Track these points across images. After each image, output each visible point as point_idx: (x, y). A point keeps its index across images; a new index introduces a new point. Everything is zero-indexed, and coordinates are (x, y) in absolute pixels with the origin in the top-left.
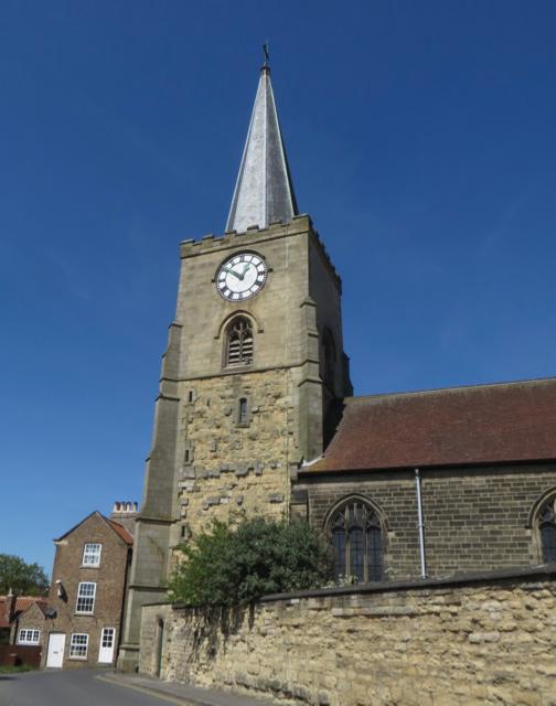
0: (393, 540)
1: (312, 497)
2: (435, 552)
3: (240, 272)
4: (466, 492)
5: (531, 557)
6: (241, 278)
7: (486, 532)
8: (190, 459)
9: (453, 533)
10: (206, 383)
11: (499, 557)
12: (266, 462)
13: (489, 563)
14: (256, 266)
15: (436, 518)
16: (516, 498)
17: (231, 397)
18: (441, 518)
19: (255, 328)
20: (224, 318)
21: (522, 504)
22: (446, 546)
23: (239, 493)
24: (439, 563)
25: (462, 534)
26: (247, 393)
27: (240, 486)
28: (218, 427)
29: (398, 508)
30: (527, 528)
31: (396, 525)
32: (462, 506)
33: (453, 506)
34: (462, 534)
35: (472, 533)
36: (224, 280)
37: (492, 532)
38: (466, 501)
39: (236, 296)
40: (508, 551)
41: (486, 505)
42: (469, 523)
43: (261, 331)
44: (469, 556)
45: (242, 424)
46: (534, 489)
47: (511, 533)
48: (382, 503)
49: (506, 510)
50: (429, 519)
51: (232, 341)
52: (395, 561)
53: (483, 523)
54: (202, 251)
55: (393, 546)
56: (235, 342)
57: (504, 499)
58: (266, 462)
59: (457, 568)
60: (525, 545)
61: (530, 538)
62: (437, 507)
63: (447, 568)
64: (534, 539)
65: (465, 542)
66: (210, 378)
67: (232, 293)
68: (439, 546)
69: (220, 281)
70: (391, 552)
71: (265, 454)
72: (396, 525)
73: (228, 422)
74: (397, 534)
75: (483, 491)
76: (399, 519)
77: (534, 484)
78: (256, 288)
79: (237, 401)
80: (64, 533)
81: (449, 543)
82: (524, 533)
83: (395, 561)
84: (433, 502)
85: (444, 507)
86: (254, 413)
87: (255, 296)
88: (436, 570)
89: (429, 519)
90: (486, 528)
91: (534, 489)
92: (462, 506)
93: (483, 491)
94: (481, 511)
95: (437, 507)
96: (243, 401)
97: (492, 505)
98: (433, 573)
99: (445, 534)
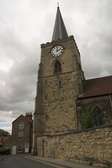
0: (105, 114)
20: (53, 61)
23: (61, 105)
26: (61, 79)
43: (63, 64)
45: (60, 87)
48: (101, 104)
52: (107, 119)
56: (57, 67)
66: (51, 76)
67: (55, 55)
69: (52, 53)
74: (106, 112)
83: (107, 119)
96: (60, 81)
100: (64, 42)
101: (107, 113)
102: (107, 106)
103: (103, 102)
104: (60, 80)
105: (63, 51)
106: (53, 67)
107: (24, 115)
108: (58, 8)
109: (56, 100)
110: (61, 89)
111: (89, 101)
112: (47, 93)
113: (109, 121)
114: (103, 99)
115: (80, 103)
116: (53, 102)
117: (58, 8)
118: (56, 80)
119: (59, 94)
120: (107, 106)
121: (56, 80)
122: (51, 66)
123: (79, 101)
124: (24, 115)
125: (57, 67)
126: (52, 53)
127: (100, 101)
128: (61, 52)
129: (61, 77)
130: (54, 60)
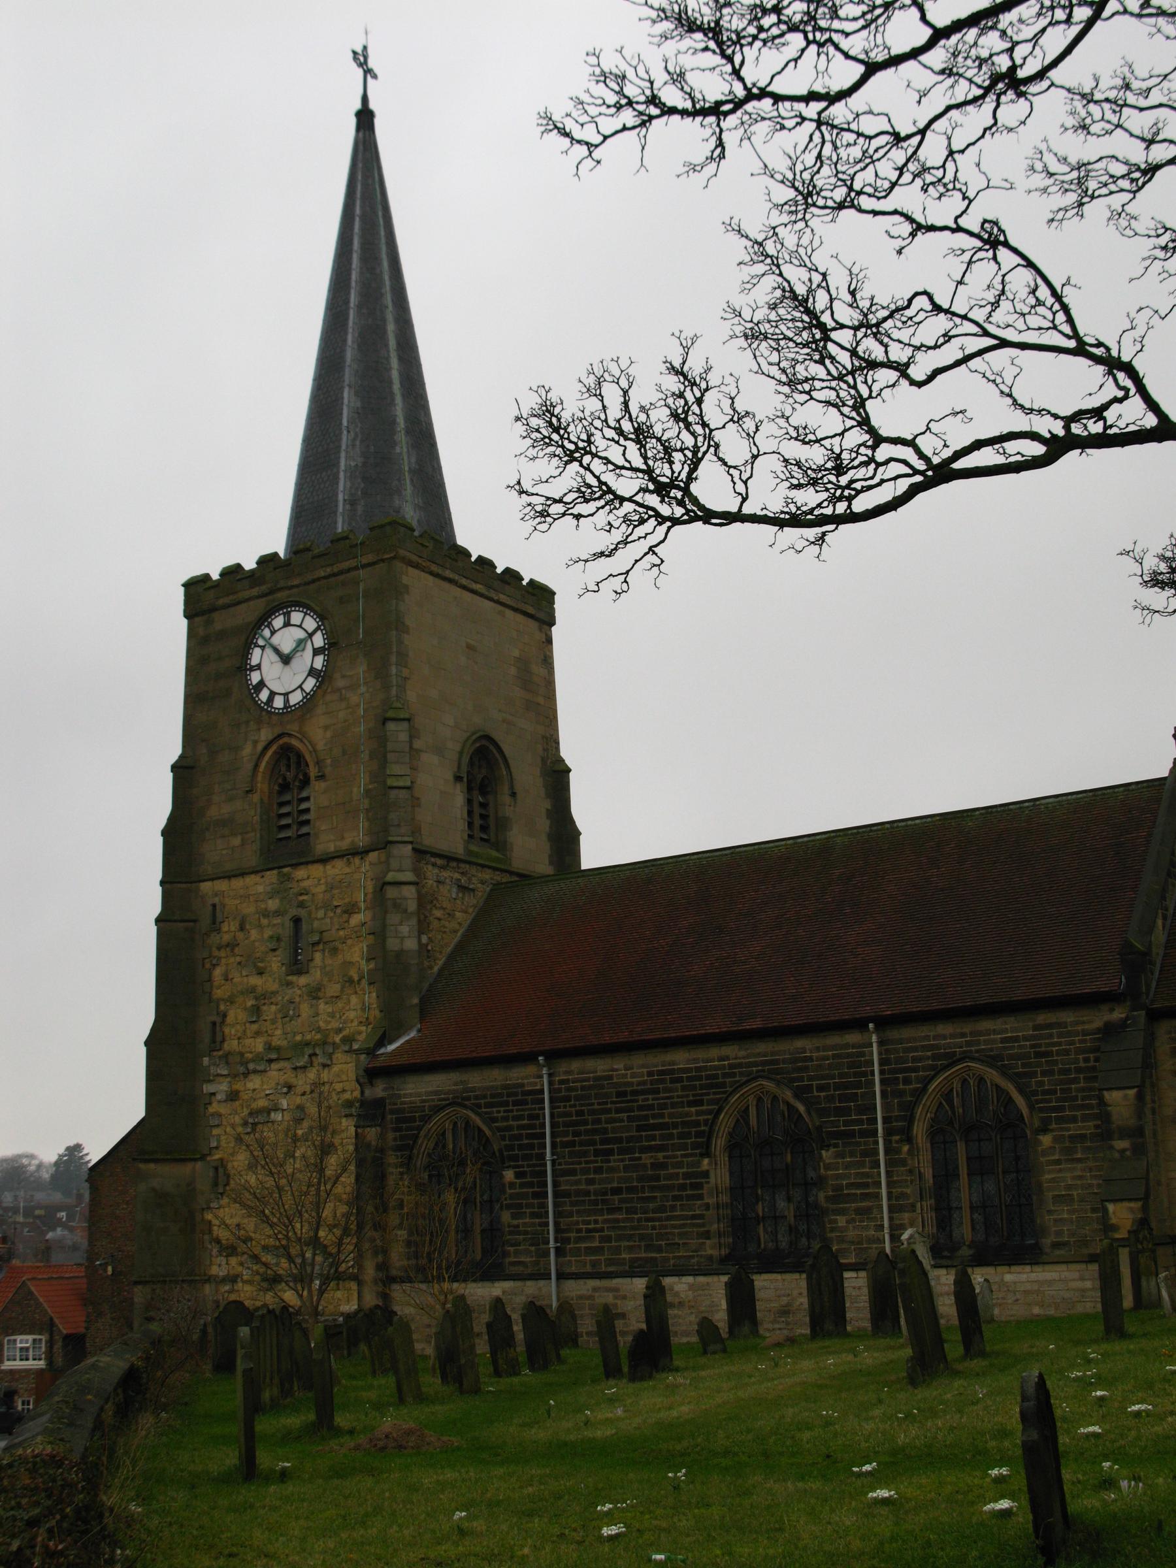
0: (512, 1185)
1: (392, 1112)
2: (573, 1204)
3: (286, 649)
4: (619, 1094)
5: (707, 1207)
6: (286, 660)
7: (645, 1165)
8: (219, 1039)
9: (598, 1170)
10: (237, 883)
11: (662, 1209)
12: (337, 1039)
13: (648, 1220)
14: (286, 695)
15: (572, 1144)
16: (691, 1104)
17: (278, 913)
18: (581, 1144)
19: (313, 771)
20: (260, 747)
21: (698, 1113)
22: (588, 1193)
23: (298, 1100)
24: (577, 1223)
25: (611, 1170)
26: (301, 905)
27: (299, 1090)
28: (261, 973)
29: (520, 1127)
30: (702, 1155)
31: (515, 1158)
32: (614, 1120)
33: (599, 1121)
34: (611, 1170)
35: (626, 1168)
36: (259, 667)
37: (654, 1166)
38: (618, 1111)
39: (279, 703)
40: (675, 1198)
41: (646, 1118)
42: (622, 1151)
43: (321, 777)
44: (620, 1209)
45: (297, 966)
46: (717, 1086)
47: (679, 1165)
48: (494, 1120)
49: (675, 1126)
50: (565, 1145)
51: (280, 793)
52: (515, 1222)
53: (644, 1150)
54: (221, 602)
55: (512, 1196)
56: (287, 797)
57: (673, 1105)
58: (337, 1039)
59: (602, 1230)
60: (699, 1186)
61: (706, 1174)
62: (576, 1124)
63: (589, 1231)
64: (712, 1174)
65: (615, 1185)
66: (243, 874)
67: (272, 694)
68: (578, 1193)
69: (252, 669)
70: (509, 1207)
71: (335, 1024)
72: (515, 1158)
73: (276, 964)
74: (518, 1175)
75: (643, 1092)
76: (521, 1147)
77: (716, 1076)
78: (310, 684)
79: (289, 924)
80: (996, 433)
81: (591, 1188)
82: (699, 1164)
83: (515, 1222)
84: (569, 1114)
85: (585, 1123)
86: (314, 944)
87: (310, 700)
88: (573, 1235)
89: (565, 1145)
90: (647, 1159)
91: (717, 1086)
92: (614, 1120)
93: (643, 1092)
94: (640, 1128)
95: (576, 1124)
96: (297, 921)
97: (654, 1116)
98: (568, 1240)
99: (585, 1171)
100: (334, 575)
101: (522, 1185)
102: (529, 1136)
103: (506, 1104)
104: (294, 912)
105: (327, 662)
106: (256, 798)
107: (249, 564)
108: (365, 118)
109: (270, 1061)
110: (303, 980)
111: (432, 1093)
112: (222, 1007)
113: (526, 1233)
114: (506, 1087)
115: (382, 1100)
116: (255, 1072)
117: (365, 118)
118: (273, 904)
119: (288, 1013)
120: (529, 1136)
121: (273, 904)
122: (247, 792)
123: (378, 1090)
124: (249, 564)
125: (287, 797)
126: (255, 677)
127: (493, 1096)
128: (312, 672)
129: (305, 884)
130: (265, 735)
